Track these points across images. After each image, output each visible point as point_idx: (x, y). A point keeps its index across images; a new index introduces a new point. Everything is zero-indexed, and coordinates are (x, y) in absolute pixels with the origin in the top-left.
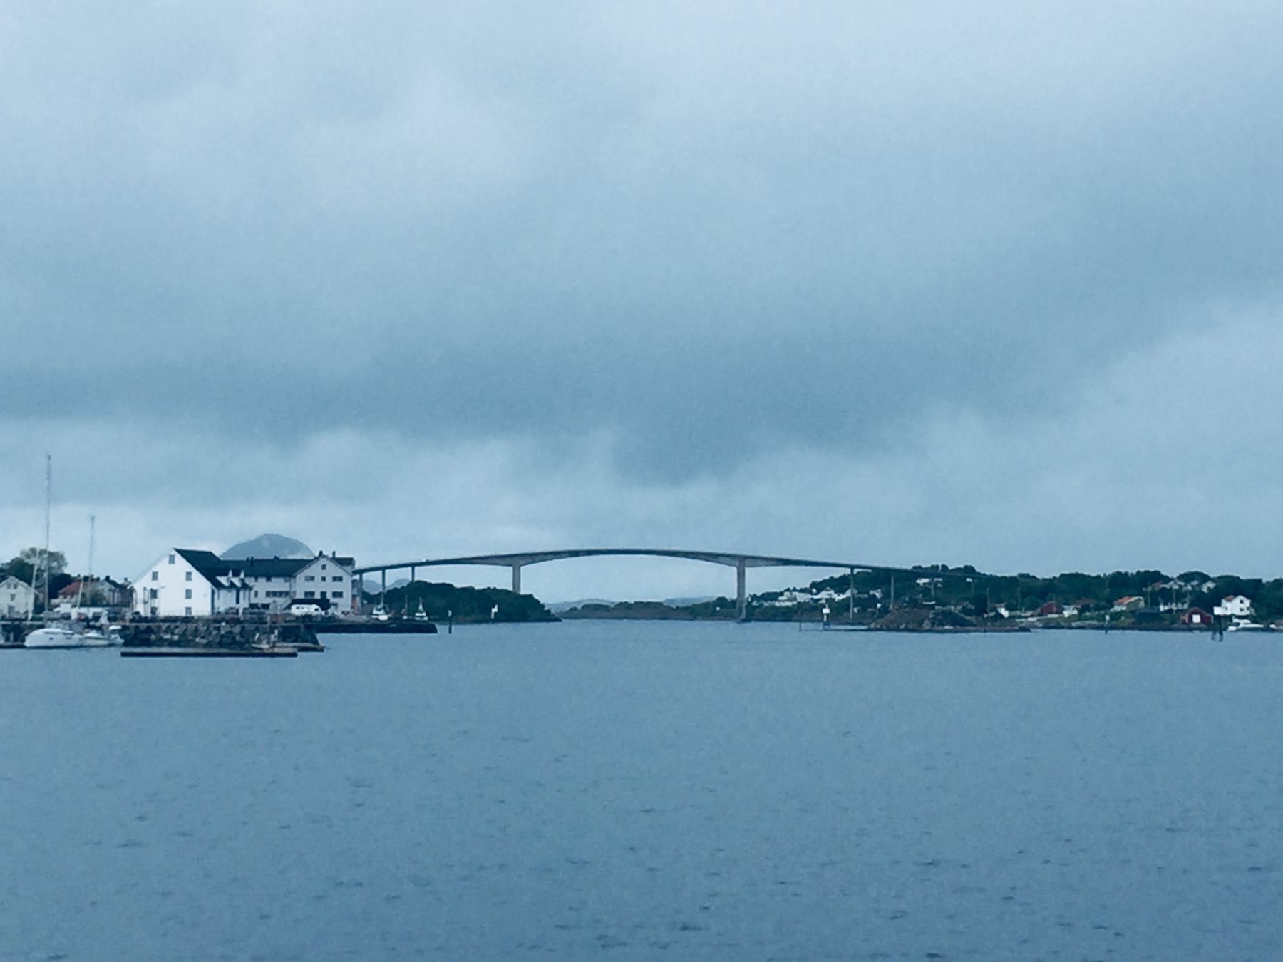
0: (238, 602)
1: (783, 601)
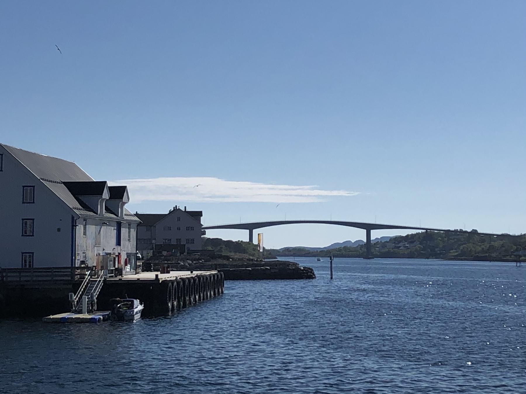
0: (119, 243)
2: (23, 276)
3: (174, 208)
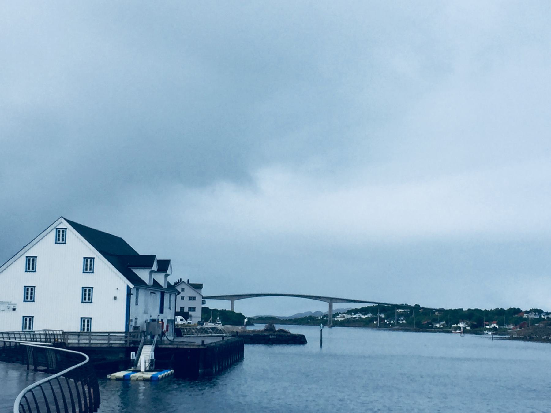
0: (162, 311)
1: (339, 318)
2: (106, 340)
3: (178, 280)
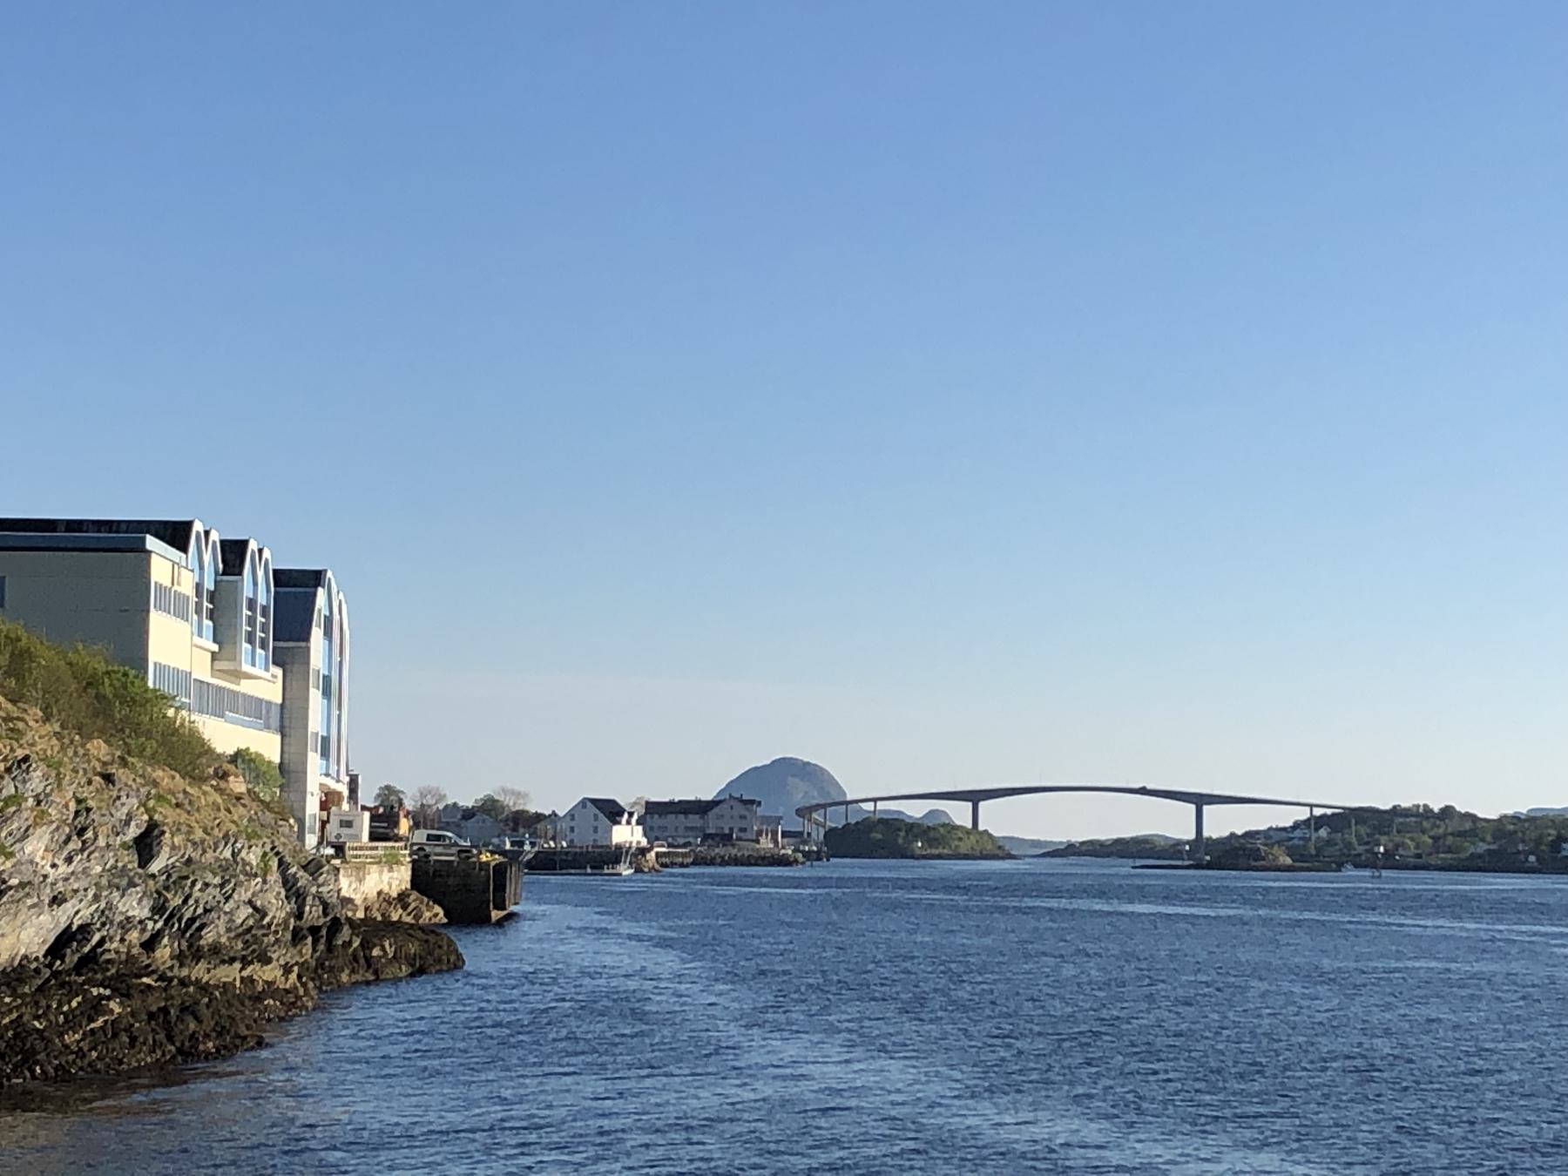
0: (632, 835)
